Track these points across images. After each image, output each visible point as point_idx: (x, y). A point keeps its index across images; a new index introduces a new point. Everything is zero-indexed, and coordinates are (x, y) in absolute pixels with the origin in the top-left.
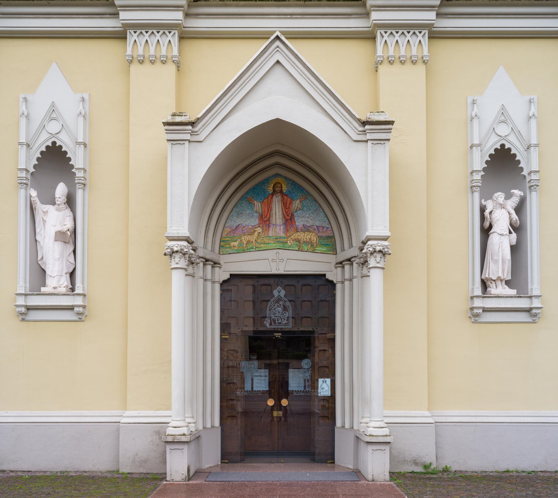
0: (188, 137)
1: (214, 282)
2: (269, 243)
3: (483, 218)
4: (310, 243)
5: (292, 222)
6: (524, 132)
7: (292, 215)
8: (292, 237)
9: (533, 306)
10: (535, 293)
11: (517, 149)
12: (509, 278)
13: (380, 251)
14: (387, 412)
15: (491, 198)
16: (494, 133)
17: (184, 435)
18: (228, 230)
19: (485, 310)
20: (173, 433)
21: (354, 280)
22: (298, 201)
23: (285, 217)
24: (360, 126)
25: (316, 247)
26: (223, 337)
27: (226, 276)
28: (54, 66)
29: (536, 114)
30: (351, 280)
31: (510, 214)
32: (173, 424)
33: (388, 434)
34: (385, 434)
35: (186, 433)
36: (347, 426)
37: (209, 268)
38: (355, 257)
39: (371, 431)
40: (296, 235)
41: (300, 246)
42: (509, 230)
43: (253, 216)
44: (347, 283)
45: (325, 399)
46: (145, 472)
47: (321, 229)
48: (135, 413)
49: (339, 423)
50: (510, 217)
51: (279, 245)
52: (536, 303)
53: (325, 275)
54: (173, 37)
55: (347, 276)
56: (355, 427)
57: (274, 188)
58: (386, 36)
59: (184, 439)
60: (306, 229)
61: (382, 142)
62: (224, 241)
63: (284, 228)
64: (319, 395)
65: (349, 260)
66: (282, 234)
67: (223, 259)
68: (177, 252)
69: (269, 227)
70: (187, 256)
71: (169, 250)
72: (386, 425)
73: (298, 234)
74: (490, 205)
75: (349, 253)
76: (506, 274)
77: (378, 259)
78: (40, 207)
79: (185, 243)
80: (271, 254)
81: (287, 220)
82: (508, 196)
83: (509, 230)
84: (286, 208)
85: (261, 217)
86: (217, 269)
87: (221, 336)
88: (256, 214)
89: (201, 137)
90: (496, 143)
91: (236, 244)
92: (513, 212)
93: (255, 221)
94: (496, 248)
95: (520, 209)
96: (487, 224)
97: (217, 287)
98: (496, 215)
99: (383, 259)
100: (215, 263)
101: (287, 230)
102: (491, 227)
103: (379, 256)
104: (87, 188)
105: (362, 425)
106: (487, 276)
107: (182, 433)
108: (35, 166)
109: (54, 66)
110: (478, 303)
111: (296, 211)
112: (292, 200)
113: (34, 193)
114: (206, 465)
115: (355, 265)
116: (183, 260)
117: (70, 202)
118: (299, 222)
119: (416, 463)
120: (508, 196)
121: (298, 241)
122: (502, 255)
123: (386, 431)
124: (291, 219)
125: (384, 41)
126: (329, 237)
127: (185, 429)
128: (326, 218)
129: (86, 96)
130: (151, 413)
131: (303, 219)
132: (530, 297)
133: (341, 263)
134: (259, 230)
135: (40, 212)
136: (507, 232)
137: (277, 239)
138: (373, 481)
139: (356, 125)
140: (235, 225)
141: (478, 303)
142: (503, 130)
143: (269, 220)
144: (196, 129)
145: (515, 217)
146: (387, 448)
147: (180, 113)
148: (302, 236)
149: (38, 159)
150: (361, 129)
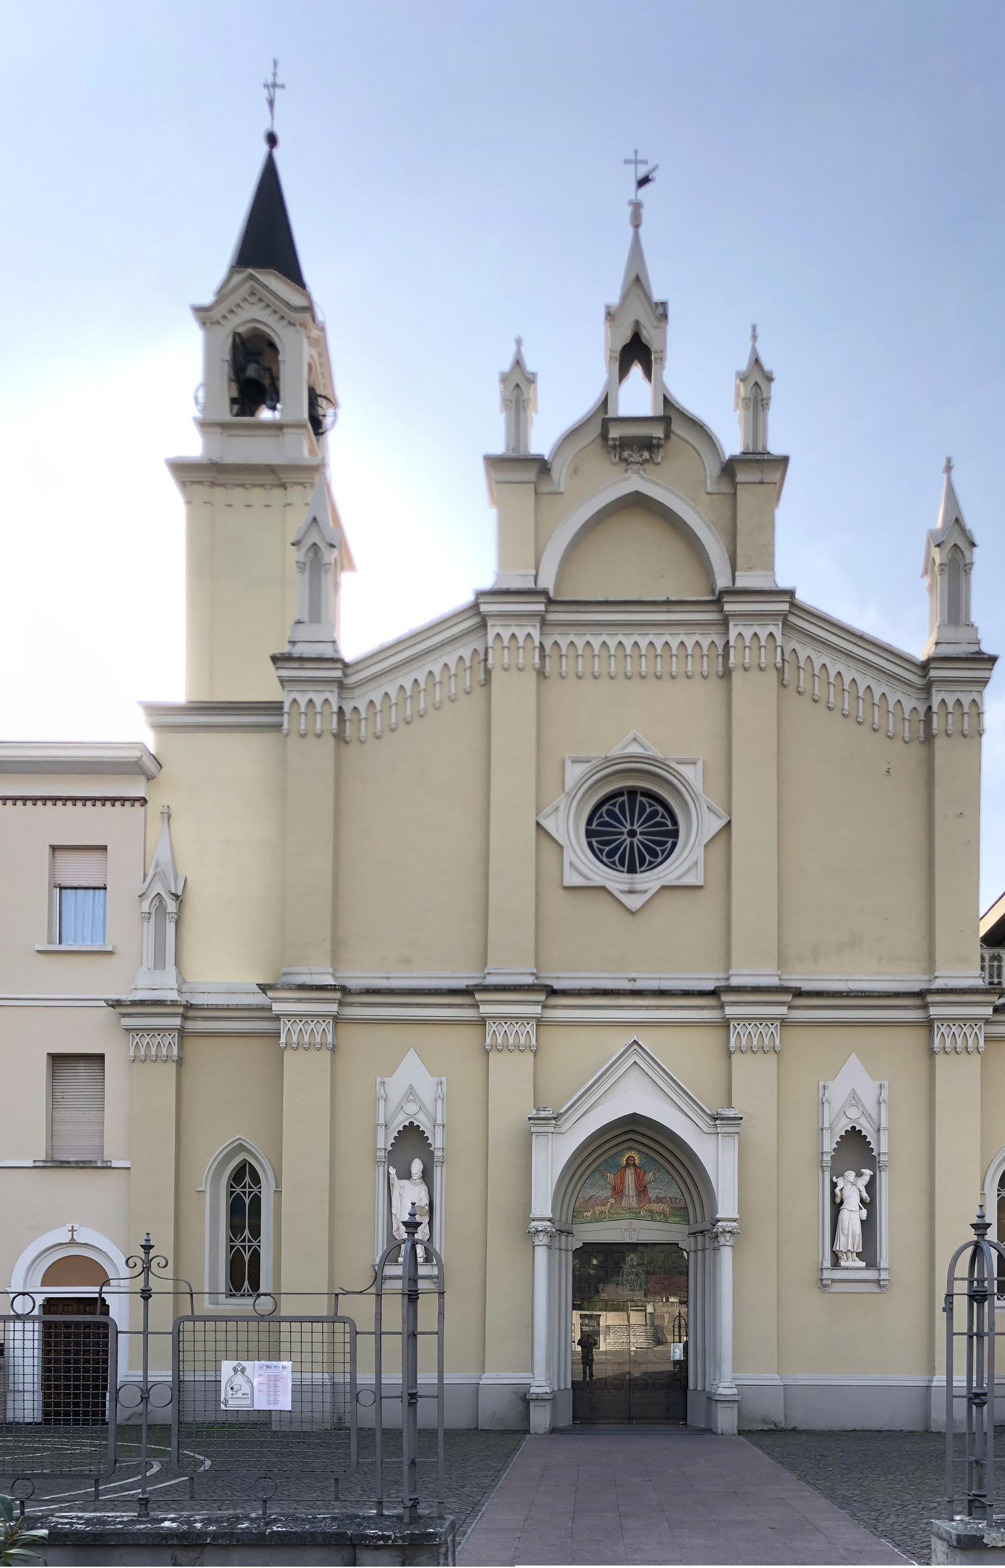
0: (552, 1130)
1: (567, 1251)
2: (622, 1214)
3: (833, 1195)
4: (662, 1213)
5: (644, 1193)
6: (874, 1116)
7: (645, 1187)
8: (645, 1208)
9: (882, 1277)
10: (882, 1266)
11: (867, 1130)
12: (860, 1250)
13: (729, 1232)
14: (737, 1375)
15: (842, 1176)
16: (845, 1116)
17: (547, 1393)
18: (580, 1200)
19: (833, 1281)
20: (537, 1392)
21: (706, 1251)
22: (651, 1174)
23: (637, 1189)
24: (711, 1120)
25: (669, 1217)
26: (575, 1303)
27: (580, 1245)
28: (412, 1052)
29: (887, 1100)
30: (703, 1250)
31: (860, 1191)
32: (538, 1383)
33: (736, 1393)
34: (733, 1393)
35: (549, 1392)
36: (699, 1388)
37: (563, 1238)
38: (708, 1230)
39: (721, 1391)
40: (648, 1207)
41: (652, 1216)
42: (860, 1207)
43: (606, 1187)
44: (700, 1253)
45: (676, 1363)
46: (503, 1429)
47: (673, 1200)
48: (493, 1375)
49: (691, 1386)
50: (860, 1194)
51: (633, 1216)
52: (884, 1275)
53: (678, 1244)
54: (531, 1028)
55: (700, 1247)
56: (707, 1389)
57: (626, 1161)
58: (738, 1028)
59: (547, 1397)
60: (659, 1200)
61: (732, 1135)
62: (576, 1211)
63: (636, 1200)
64: (223, 1407)
65: (702, 1232)
66: (635, 1205)
67: (576, 1228)
68: (541, 1231)
69: (622, 1197)
70: (549, 1234)
71: (533, 1230)
72: (734, 1386)
73: (651, 1204)
74: (840, 1183)
75: (700, 1227)
76: (856, 1247)
77: (728, 1238)
78: (396, 1183)
79: (549, 1223)
80: (624, 1224)
81: (640, 1192)
82: (859, 1175)
83: (860, 1207)
84: (638, 1180)
85: (614, 1188)
86: (570, 1238)
87: (573, 1301)
88: (609, 1186)
89: (564, 1129)
90: (846, 1125)
91: (589, 1214)
92: (863, 1190)
93: (609, 1193)
94: (846, 1223)
95: (871, 1187)
96: (838, 1200)
97: (570, 1254)
98: (846, 1192)
99: (732, 1238)
100: (569, 1233)
101: (639, 1201)
102: (842, 1202)
103: (728, 1235)
104: (445, 1165)
105: (713, 1386)
106: (838, 1249)
107: (545, 1392)
108: (392, 1145)
109: (412, 1052)
110: (827, 1274)
111: (650, 1183)
112: (645, 1172)
113: (392, 1171)
114: (561, 1425)
115: (707, 1238)
116: (546, 1237)
117: (427, 1177)
118: (652, 1194)
119: (765, 1422)
120: (859, 1175)
121: (651, 1211)
122: (853, 1229)
123: (735, 1391)
124: (643, 1191)
125: (737, 1032)
126: (681, 1208)
127: (548, 1388)
128: (679, 1190)
129: (444, 1079)
130: (509, 1374)
131: (656, 1191)
132: (879, 1269)
133: (694, 1233)
134: (612, 1201)
135: (398, 1187)
136: (858, 1208)
137: (630, 1210)
138: (722, 1434)
139: (707, 1119)
140: (588, 1196)
141: (827, 1274)
142: (853, 1113)
143: (622, 1191)
144: (558, 1123)
145: (865, 1195)
146: (736, 1405)
147: (543, 1108)
148: (656, 1207)
149: (395, 1138)
150: (713, 1123)
